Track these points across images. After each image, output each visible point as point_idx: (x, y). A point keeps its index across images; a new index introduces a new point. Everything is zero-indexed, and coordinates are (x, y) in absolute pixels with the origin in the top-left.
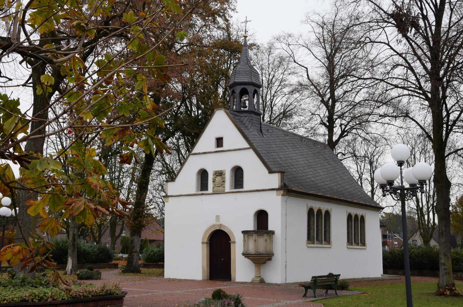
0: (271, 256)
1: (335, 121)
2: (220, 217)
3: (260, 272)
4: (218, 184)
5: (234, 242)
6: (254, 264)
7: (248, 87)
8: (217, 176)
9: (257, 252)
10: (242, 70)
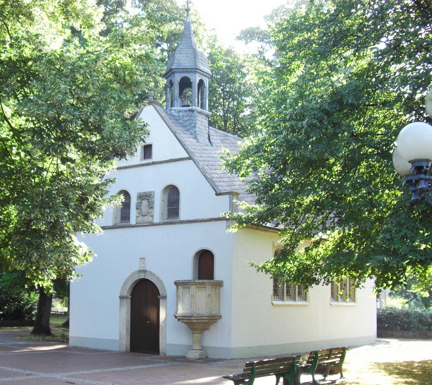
0: (217, 319)
5: (165, 297)
7: (189, 74)
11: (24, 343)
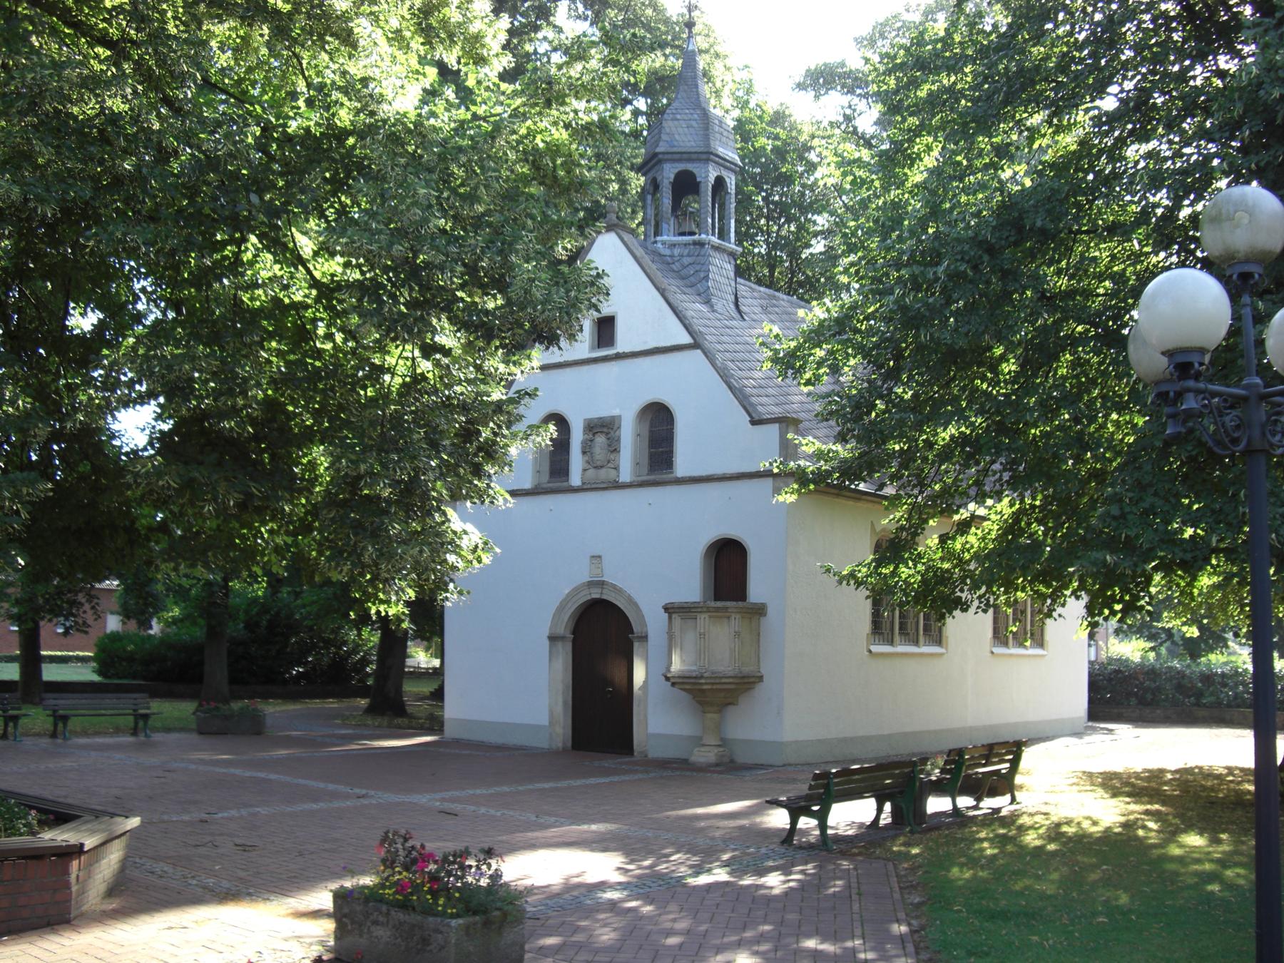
5: (644, 638)
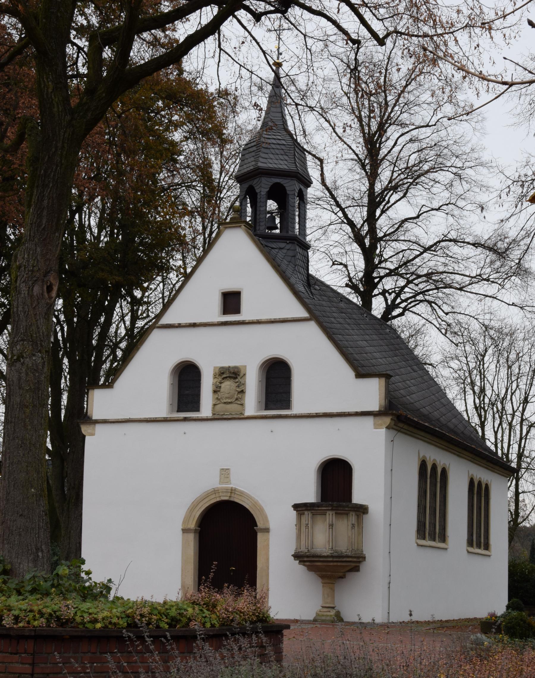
0: (360, 562)
1: (378, 282)
2: (232, 472)
3: (333, 597)
4: (226, 398)
5: (267, 530)
6: (320, 580)
8: (223, 379)
9: (336, 552)
10: (274, 141)
11: (483, 499)
